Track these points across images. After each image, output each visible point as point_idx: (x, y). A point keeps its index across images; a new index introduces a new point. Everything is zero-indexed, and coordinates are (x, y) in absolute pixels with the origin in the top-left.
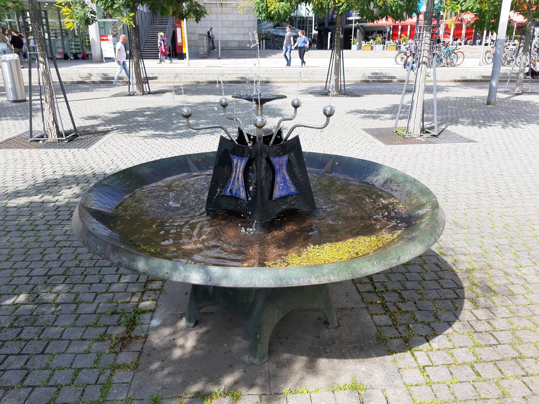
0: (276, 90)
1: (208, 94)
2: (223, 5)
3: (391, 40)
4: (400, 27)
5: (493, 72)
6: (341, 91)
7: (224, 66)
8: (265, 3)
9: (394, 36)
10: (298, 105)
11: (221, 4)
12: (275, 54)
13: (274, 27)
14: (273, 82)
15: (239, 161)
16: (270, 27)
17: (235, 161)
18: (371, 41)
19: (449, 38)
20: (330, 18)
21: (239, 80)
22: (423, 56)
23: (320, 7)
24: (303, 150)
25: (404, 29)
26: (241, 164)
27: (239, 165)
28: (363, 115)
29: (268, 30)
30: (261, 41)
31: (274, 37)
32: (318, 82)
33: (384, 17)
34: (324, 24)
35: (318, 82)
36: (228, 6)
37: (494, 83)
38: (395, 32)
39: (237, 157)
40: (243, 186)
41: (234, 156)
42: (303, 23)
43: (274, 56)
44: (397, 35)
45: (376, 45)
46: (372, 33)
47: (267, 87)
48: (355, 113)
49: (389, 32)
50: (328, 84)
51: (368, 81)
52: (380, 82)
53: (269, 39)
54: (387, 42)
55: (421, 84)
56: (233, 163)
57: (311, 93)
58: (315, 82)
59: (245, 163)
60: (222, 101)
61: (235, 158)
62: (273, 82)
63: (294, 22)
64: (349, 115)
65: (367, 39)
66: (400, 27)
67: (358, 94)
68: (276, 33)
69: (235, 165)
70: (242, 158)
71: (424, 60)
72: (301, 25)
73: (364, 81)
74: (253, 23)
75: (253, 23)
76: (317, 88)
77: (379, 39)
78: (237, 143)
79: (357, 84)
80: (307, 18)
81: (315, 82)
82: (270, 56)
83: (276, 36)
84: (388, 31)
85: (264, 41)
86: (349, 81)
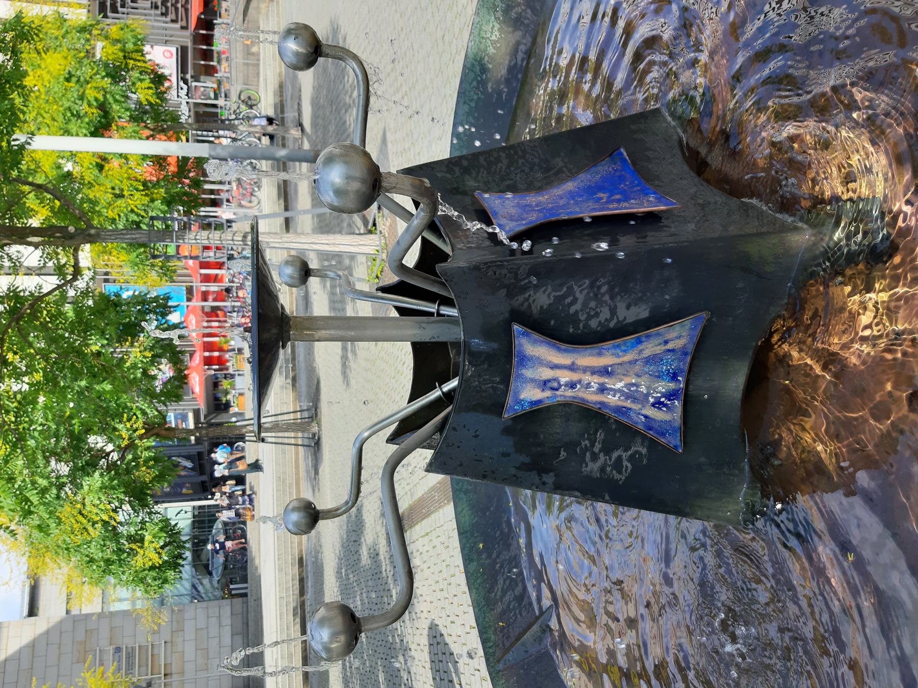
0: (314, 541)
1: (328, 680)
2: (168, 672)
3: (228, 364)
4: (207, 354)
5: (267, 158)
6: (312, 417)
7: (275, 657)
8: (146, 572)
9: (221, 362)
10: (298, 264)
11: (165, 675)
12: (253, 560)
13: (210, 574)
14: (301, 551)
15: (528, 373)
16: (211, 582)
17: (530, 394)
18: (229, 397)
19: (222, 275)
20: (193, 473)
21: (298, 620)
22: (233, 240)
23: (152, 463)
24: (446, 155)
25: (209, 347)
26: (540, 362)
27: (546, 374)
28: (350, 355)
29: (216, 585)
30: (233, 592)
31: (227, 571)
32: (297, 467)
33: (179, 358)
34: (203, 483)
35: (297, 467)
36: (169, 661)
37: (282, 153)
38: (216, 362)
39: (512, 386)
40: (639, 341)
41: (510, 400)
42: (203, 522)
43: (257, 561)
44: (219, 357)
45: (237, 387)
46: (217, 399)
47: (309, 563)
48: (348, 371)
49: (215, 370)
50: (300, 442)
51: (294, 379)
52: (294, 359)
53: (231, 579)
54: (231, 371)
55: (285, 239)
56: (540, 401)
57: (316, 472)
58: (297, 474)
59: (535, 342)
60: (296, 524)
61: (517, 394)
62: (301, 551)
63: (202, 538)
64: (353, 382)
65: (227, 405)
66: (207, 354)
67: (314, 387)
68: (221, 568)
69: (548, 393)
70: (515, 360)
71: (240, 239)
72: (207, 525)
73: (294, 385)
74: (199, 610)
75: (199, 610)
76: (307, 465)
77: (225, 384)
78: (450, 408)
79: (298, 398)
80: (194, 516)
81: (297, 474)
82: (257, 568)
83: (225, 567)
84: (213, 372)
85: (232, 587)
86: (295, 405)
